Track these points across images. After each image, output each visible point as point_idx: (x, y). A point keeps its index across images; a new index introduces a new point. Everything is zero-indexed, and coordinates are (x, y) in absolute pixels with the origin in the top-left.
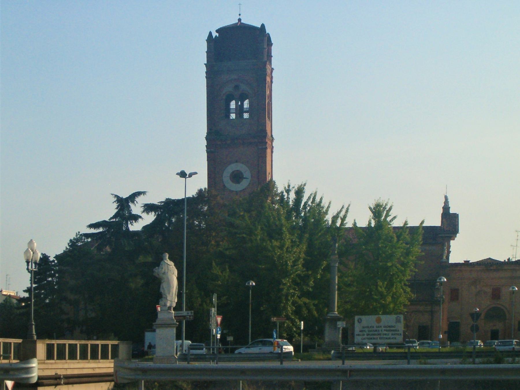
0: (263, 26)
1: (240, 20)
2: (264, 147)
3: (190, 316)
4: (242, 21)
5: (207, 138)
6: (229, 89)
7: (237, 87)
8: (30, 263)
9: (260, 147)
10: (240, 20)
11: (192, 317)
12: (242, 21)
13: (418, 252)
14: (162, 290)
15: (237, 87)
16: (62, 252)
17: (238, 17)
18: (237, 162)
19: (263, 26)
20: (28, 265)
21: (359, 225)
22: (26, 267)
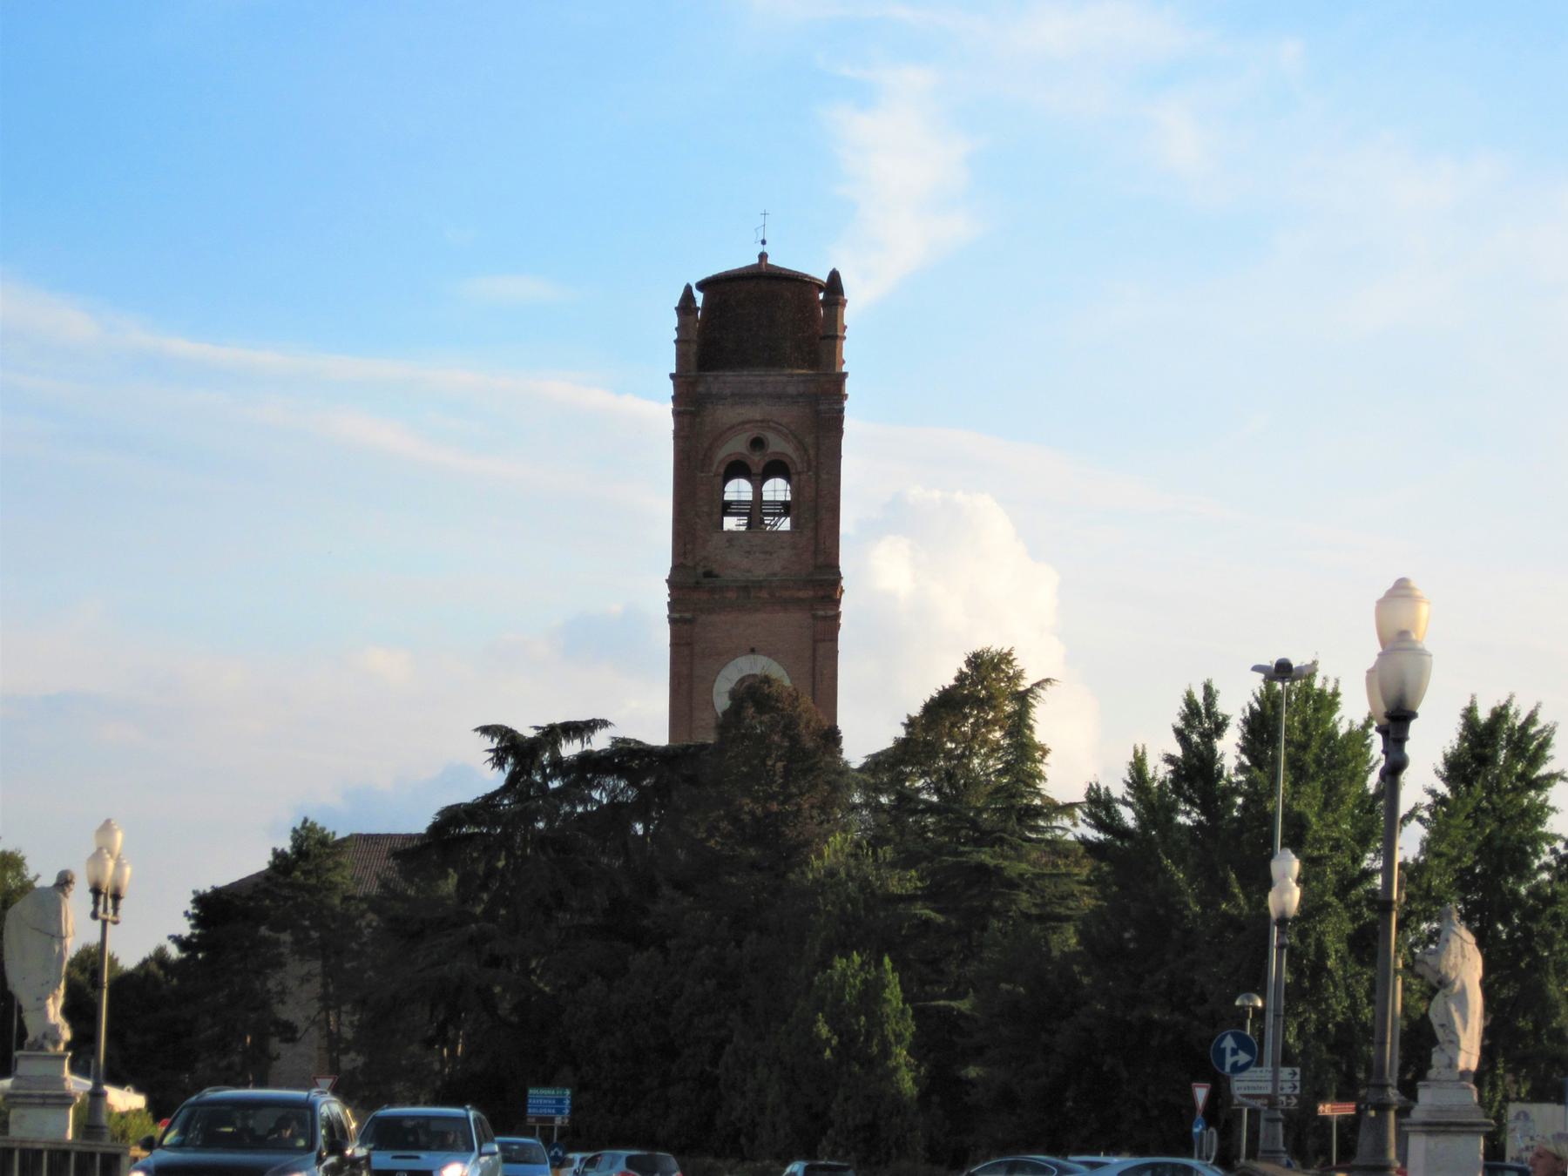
0: (835, 276)
1: (763, 256)
2: (831, 613)
3: (1288, 1097)
4: (770, 261)
5: (672, 582)
6: (736, 446)
7: (758, 443)
8: (102, 898)
9: (821, 613)
10: (763, 256)
11: (1294, 1101)
12: (770, 261)
13: (1320, 922)
14: (10, 988)
15: (758, 443)
16: (890, 744)
17: (760, 249)
18: (753, 651)
19: (835, 276)
20: (96, 903)
21: (1556, 795)
22: (91, 908)
